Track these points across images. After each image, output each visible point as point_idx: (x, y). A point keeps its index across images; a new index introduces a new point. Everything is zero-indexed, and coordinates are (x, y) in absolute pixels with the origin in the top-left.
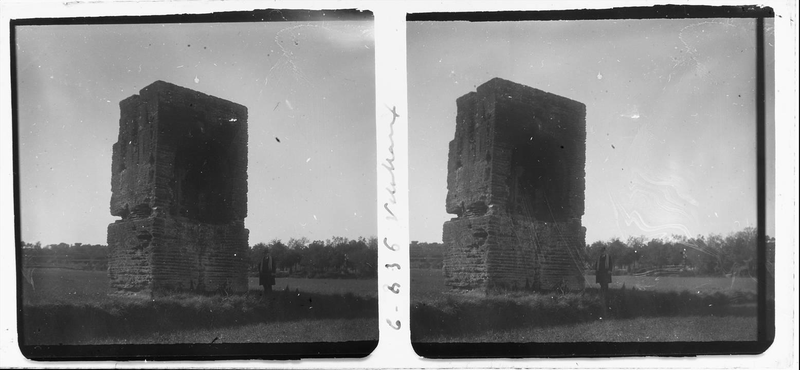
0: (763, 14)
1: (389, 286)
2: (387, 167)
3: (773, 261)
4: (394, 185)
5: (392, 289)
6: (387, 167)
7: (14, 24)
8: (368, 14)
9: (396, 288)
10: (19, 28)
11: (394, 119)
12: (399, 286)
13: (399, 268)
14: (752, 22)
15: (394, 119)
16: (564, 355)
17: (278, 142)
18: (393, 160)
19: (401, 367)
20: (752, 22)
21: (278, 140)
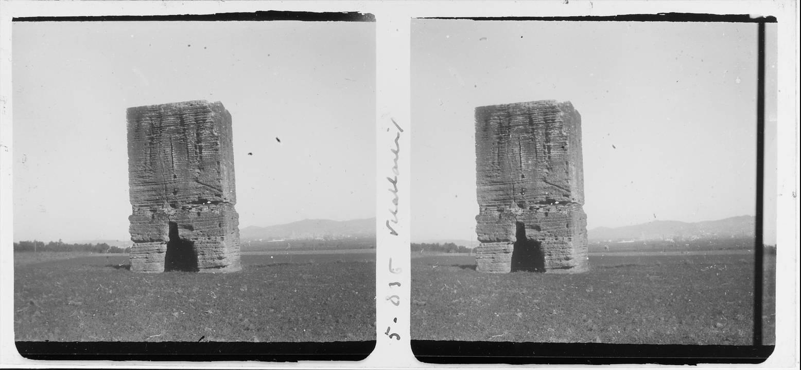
21: (279, 140)
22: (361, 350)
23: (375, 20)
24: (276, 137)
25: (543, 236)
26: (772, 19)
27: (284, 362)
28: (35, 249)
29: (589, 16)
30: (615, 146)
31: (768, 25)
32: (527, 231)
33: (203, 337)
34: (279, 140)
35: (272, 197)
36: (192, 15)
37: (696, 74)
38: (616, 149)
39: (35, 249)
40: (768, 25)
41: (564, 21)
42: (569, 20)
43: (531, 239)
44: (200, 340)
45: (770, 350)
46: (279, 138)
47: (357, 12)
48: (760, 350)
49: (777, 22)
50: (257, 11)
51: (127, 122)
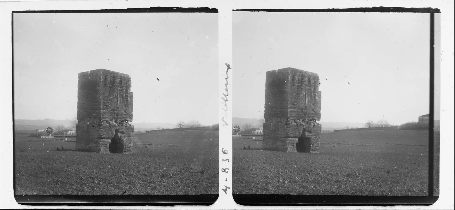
0: (432, 12)
1: (224, 118)
2: (224, 99)
3: (438, 160)
4: (227, 90)
5: (227, 124)
6: (224, 99)
7: (13, 12)
8: (215, 11)
9: (227, 170)
10: (14, 14)
11: (228, 70)
12: (229, 170)
13: (229, 161)
14: (428, 15)
15: (228, 70)
16: (17, 157)
17: (158, 81)
18: (227, 95)
19: (223, 209)
20: (428, 15)
21: (158, 80)
22: (210, 199)
23: (218, 12)
24: (156, 78)
25: (312, 136)
26: (438, 11)
27: (167, 206)
28: (225, 180)
29: (107, 9)
30: (349, 83)
31: (436, 14)
32: (307, 133)
33: (125, 192)
34: (158, 80)
35: (151, 112)
36: (114, 9)
37: (396, 42)
38: (350, 85)
39: (225, 180)
40: (436, 14)
41: (319, 12)
42: (249, 11)
43: (308, 137)
44: (124, 194)
45: (436, 198)
46: (158, 78)
47: (430, 8)
48: (431, 198)
49: (440, 12)
50: (215, 8)
51: (130, 76)
